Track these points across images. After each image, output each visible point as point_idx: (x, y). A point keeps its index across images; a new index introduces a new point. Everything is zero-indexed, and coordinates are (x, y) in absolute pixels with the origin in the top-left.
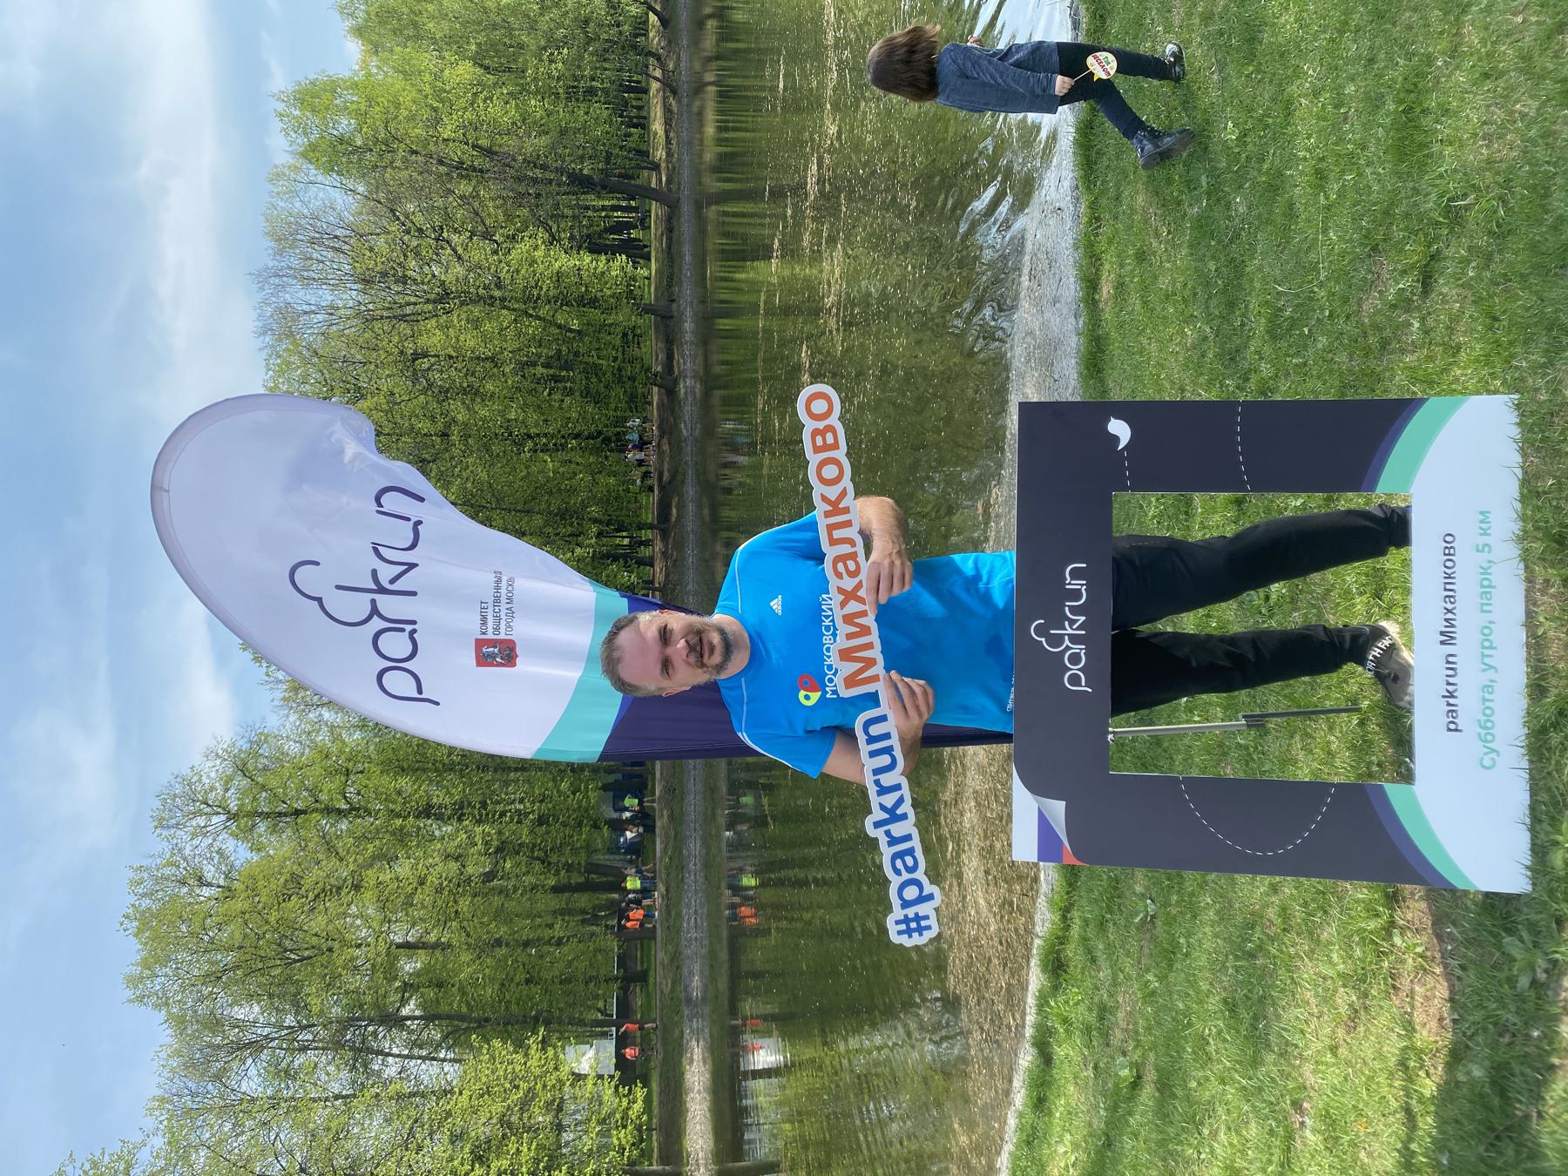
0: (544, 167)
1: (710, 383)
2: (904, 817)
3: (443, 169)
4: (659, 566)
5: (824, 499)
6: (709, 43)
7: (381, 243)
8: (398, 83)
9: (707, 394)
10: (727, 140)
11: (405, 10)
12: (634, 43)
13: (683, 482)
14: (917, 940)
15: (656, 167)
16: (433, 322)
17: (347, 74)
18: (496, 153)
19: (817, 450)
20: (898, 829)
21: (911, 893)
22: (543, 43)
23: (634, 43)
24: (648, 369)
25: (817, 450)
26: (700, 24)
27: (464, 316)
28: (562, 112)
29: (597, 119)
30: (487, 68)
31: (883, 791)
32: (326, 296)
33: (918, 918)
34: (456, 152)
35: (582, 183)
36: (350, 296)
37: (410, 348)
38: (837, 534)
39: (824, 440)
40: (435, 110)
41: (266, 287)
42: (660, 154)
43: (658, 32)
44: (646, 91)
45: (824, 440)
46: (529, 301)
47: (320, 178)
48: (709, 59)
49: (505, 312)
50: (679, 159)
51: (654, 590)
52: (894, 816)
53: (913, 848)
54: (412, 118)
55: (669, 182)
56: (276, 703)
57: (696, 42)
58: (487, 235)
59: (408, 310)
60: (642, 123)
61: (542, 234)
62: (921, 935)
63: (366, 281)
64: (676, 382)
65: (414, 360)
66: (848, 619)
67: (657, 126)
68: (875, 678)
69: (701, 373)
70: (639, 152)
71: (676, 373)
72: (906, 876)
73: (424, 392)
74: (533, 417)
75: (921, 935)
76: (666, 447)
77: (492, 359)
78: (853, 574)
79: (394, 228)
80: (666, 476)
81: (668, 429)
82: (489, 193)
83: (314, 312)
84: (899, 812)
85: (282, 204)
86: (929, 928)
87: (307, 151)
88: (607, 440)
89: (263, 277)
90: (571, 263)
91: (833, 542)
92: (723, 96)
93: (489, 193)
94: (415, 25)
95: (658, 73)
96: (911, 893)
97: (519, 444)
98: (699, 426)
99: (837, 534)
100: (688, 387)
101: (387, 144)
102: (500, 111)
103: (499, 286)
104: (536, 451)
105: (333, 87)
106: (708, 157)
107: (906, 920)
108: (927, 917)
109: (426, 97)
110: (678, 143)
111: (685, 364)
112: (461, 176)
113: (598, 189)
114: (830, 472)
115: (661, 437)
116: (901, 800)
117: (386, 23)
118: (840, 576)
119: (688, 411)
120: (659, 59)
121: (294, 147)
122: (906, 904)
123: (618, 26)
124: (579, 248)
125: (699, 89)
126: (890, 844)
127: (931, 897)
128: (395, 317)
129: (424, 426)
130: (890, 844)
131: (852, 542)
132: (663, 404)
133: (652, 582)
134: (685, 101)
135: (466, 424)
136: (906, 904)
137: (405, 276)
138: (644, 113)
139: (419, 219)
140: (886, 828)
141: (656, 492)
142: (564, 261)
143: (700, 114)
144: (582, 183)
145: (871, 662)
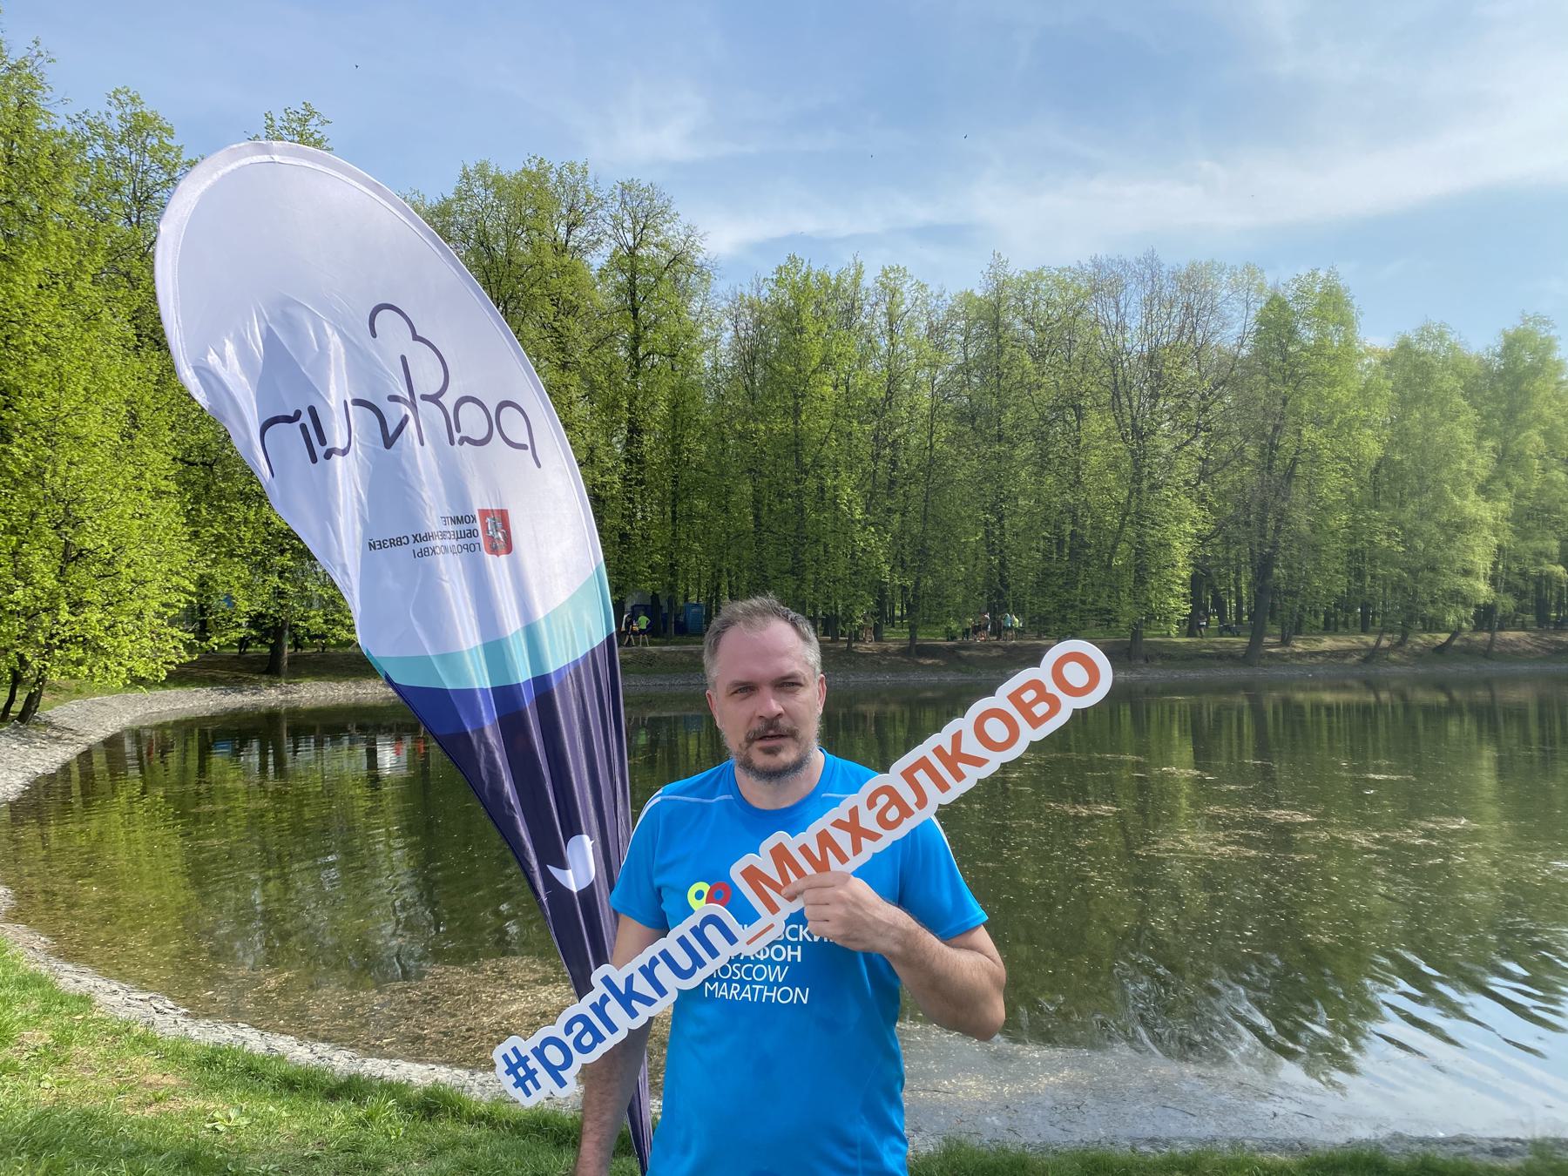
0: (1278, 530)
2: (633, 1014)
5: (957, 738)
6: (1422, 696)
8: (1356, 385)
15: (1285, 641)
19: (1015, 698)
20: (614, 1009)
21: (554, 1055)
23: (1413, 617)
25: (1015, 698)
26: (1442, 687)
27: (1120, 453)
28: (1335, 546)
29: (1331, 581)
30: (1376, 471)
31: (648, 972)
32: (1135, 322)
33: (531, 1074)
34: (1287, 442)
35: (1263, 567)
36: (1134, 342)
38: (921, 776)
40: (1330, 422)
42: (1299, 646)
44: (1364, 631)
47: (1253, 313)
48: (1403, 697)
52: (627, 998)
54: (1320, 399)
55: (1271, 654)
57: (1422, 682)
58: (1203, 475)
60: (1330, 628)
61: (1207, 528)
62: (516, 1085)
63: (1151, 360)
65: (1074, 407)
66: (824, 839)
67: (1328, 643)
68: (773, 908)
72: (569, 1041)
73: (1043, 418)
74: (1021, 522)
75: (516, 1085)
78: (881, 819)
82: (1247, 475)
84: (635, 1003)
86: (528, 1093)
90: (1179, 558)
91: (908, 775)
93: (1247, 475)
94: (1417, 399)
96: (554, 1055)
99: (921, 776)
102: (1333, 484)
104: (986, 524)
105: (1345, 322)
107: (523, 1061)
108: (538, 1086)
112: (1263, 447)
116: (649, 1001)
118: (871, 803)
120: (1400, 644)
122: (539, 1053)
125: (1371, 685)
126: (593, 1007)
127: (561, 1083)
128: (1116, 388)
129: (1009, 417)
134: (1357, 672)
135: (1011, 457)
137: (1158, 396)
138: (1341, 629)
140: (609, 995)
142: (1181, 552)
143: (1345, 688)
144: (1263, 567)
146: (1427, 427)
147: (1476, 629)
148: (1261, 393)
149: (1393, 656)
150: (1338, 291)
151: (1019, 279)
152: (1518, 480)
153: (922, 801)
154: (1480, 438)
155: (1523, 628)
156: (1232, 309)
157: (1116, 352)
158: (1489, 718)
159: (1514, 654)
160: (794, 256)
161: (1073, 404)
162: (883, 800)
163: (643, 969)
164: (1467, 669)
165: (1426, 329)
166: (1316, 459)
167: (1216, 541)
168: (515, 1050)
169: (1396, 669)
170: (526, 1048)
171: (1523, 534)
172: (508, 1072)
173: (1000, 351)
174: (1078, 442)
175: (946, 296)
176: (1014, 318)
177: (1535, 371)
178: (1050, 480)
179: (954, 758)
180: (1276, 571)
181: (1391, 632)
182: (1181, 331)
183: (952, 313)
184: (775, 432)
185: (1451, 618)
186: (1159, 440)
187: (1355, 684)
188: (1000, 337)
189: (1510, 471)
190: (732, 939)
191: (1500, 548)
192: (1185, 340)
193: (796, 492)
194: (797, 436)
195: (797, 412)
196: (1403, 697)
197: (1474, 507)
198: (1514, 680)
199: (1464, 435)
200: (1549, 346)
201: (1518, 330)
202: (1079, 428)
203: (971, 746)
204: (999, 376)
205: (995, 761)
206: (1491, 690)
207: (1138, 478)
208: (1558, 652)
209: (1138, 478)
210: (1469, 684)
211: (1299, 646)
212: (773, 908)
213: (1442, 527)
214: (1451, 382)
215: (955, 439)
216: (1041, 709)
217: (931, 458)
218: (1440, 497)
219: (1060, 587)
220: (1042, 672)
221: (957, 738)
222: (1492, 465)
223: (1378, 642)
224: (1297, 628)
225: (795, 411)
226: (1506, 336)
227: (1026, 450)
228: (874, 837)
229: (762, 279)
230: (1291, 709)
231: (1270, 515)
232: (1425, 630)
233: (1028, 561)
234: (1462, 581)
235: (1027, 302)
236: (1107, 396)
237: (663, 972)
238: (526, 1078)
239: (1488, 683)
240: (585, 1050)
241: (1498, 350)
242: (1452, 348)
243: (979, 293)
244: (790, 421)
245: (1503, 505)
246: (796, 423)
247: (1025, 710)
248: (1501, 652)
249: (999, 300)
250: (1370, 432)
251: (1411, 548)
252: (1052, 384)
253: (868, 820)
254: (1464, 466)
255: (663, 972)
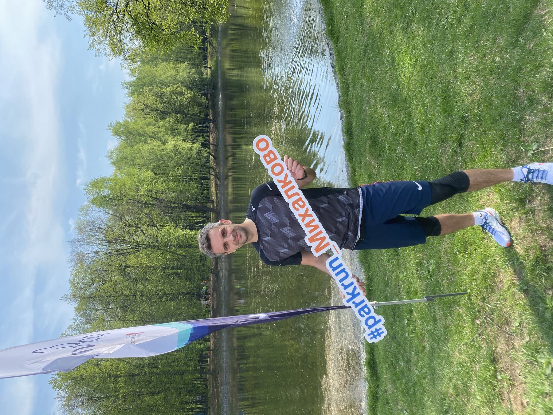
0: (174, 203)
1: (231, 272)
2: (359, 294)
3: (139, 205)
4: (212, 341)
5: (279, 181)
6: (230, 162)
7: (116, 230)
8: (126, 178)
9: (230, 275)
10: (237, 194)
11: (130, 156)
12: (205, 165)
13: (221, 308)
14: (379, 339)
15: (213, 202)
16: (133, 255)
17: (108, 176)
18: (158, 199)
19: (268, 163)
20: (357, 300)
21: (371, 322)
22: (175, 165)
23: (205, 165)
24: (209, 268)
25: (268, 163)
26: (227, 159)
27: (144, 253)
28: (181, 186)
29: (193, 187)
30: (156, 174)
31: (346, 287)
32: (95, 248)
33: (377, 330)
34: (144, 199)
35: (188, 208)
36: (104, 248)
37: (124, 264)
38: (290, 193)
39: (270, 158)
40: (138, 186)
41: (74, 246)
42: (214, 198)
43: (213, 161)
44: (209, 179)
45: (270, 158)
46: (167, 247)
47: (97, 209)
48: (230, 169)
49: (159, 251)
50: (220, 199)
51: (210, 351)
52: (354, 295)
53: (366, 305)
54: (130, 189)
55: (217, 206)
56: (60, 406)
57: (225, 164)
58: (154, 225)
59: (125, 251)
60: (209, 189)
61: (173, 225)
62: (380, 336)
63: (110, 242)
64: (219, 272)
65: (125, 269)
66: (307, 225)
67: (213, 189)
68: (328, 244)
69: (228, 268)
70: (207, 197)
71: (219, 269)
72: (367, 316)
73: (127, 280)
74: (167, 287)
75: (380, 336)
76: (215, 296)
77: (153, 267)
78: (303, 207)
79: (121, 224)
80: (215, 307)
81: (216, 289)
82: (155, 213)
83: (90, 254)
84: (356, 293)
85: (83, 218)
86: (383, 332)
87: (92, 200)
88: (193, 294)
89: (74, 242)
90: (183, 233)
91: (289, 197)
92: (234, 179)
93: (155, 213)
94: (133, 161)
95: (213, 173)
96: (371, 322)
97: (161, 298)
98: (227, 287)
99: (290, 193)
100: (223, 273)
101: (121, 197)
102: (160, 186)
103: (157, 241)
104: (167, 300)
105: (103, 180)
106: (230, 198)
107: (372, 333)
108: (380, 329)
109: (135, 182)
110: (220, 194)
111: (222, 265)
112: (146, 207)
113: (193, 209)
114: (277, 169)
115: (213, 292)
116: (355, 288)
117: (123, 160)
118: (297, 209)
119: (223, 282)
120: (213, 169)
121: (88, 199)
122: (370, 327)
123: (200, 159)
124: (186, 228)
125: (226, 177)
126: (356, 307)
127: (380, 321)
128: (119, 254)
129: (127, 293)
130: (356, 307)
131: (297, 194)
132: (214, 280)
133: (209, 348)
134: (222, 181)
135: (142, 291)
136: (370, 327)
137: (123, 240)
138: (209, 186)
139: (131, 221)
140: (352, 301)
141: (211, 312)
142: (180, 232)
143: (227, 185)
144: (188, 208)
145: (323, 239)
146: (142, 157)
147: (209, 148)
148: (126, 207)
149: (218, 171)
150: (92, 183)
151: (73, 290)
152: (162, 134)
153: (297, 194)
154: (147, 143)
155: (209, 136)
156: (94, 216)
157: (106, 254)
158: (236, 145)
159: (217, 139)
160: (49, 382)
161: (124, 270)
162: (296, 206)
163: (345, 289)
164: (221, 151)
165: (109, 157)
166: (150, 191)
167: (177, 222)
168: (369, 335)
169: (221, 170)
170: (368, 331)
171: (179, 134)
172: (376, 338)
173: (101, 297)
174: (138, 267)
175: (76, 318)
176: (88, 291)
177: (127, 127)
178: (152, 277)
179: (285, 183)
180: (189, 204)
181: (210, 172)
182: (100, 232)
183: (83, 315)
184: (124, 385)
185: (205, 154)
186: (140, 240)
187: (225, 183)
188: (95, 296)
189: (159, 136)
190: (337, 259)
191: (184, 140)
192: (105, 231)
193: (149, 375)
194: (126, 376)
195: (116, 376)
196: (230, 169)
197: (170, 146)
198: (225, 140)
199: (146, 147)
200: (119, 123)
201: (112, 132)
202: (133, 267)
203: (282, 177)
204: (110, 296)
205: (286, 171)
206: (227, 145)
207: (154, 247)
208: (216, 128)
209: (154, 247)
210: (226, 151)
211: (214, 198)
212: (328, 244)
213: (175, 154)
214: (128, 151)
215: (133, 312)
216: (272, 156)
217: (140, 320)
218: (166, 155)
219: (192, 273)
220: (262, 154)
221: (279, 181)
222: (156, 141)
223: (213, 175)
224: (208, 199)
225: (116, 377)
226: (114, 135)
227: (140, 286)
228: (307, 210)
229: (57, 396)
230: (235, 201)
231: (169, 204)
232: (209, 163)
233: (182, 284)
234: (194, 151)
235: (82, 287)
236: (122, 257)
237: (346, 282)
238: (378, 333)
239: (226, 146)
240: (370, 312)
241: (118, 137)
242: (116, 150)
243: (76, 305)
244: (120, 379)
245: (170, 138)
246: (121, 376)
247: (272, 160)
248: (216, 142)
249: (80, 297)
250: (142, 174)
251: (182, 164)
252: (116, 277)
253: (302, 211)
254: (156, 148)
255: (346, 282)
